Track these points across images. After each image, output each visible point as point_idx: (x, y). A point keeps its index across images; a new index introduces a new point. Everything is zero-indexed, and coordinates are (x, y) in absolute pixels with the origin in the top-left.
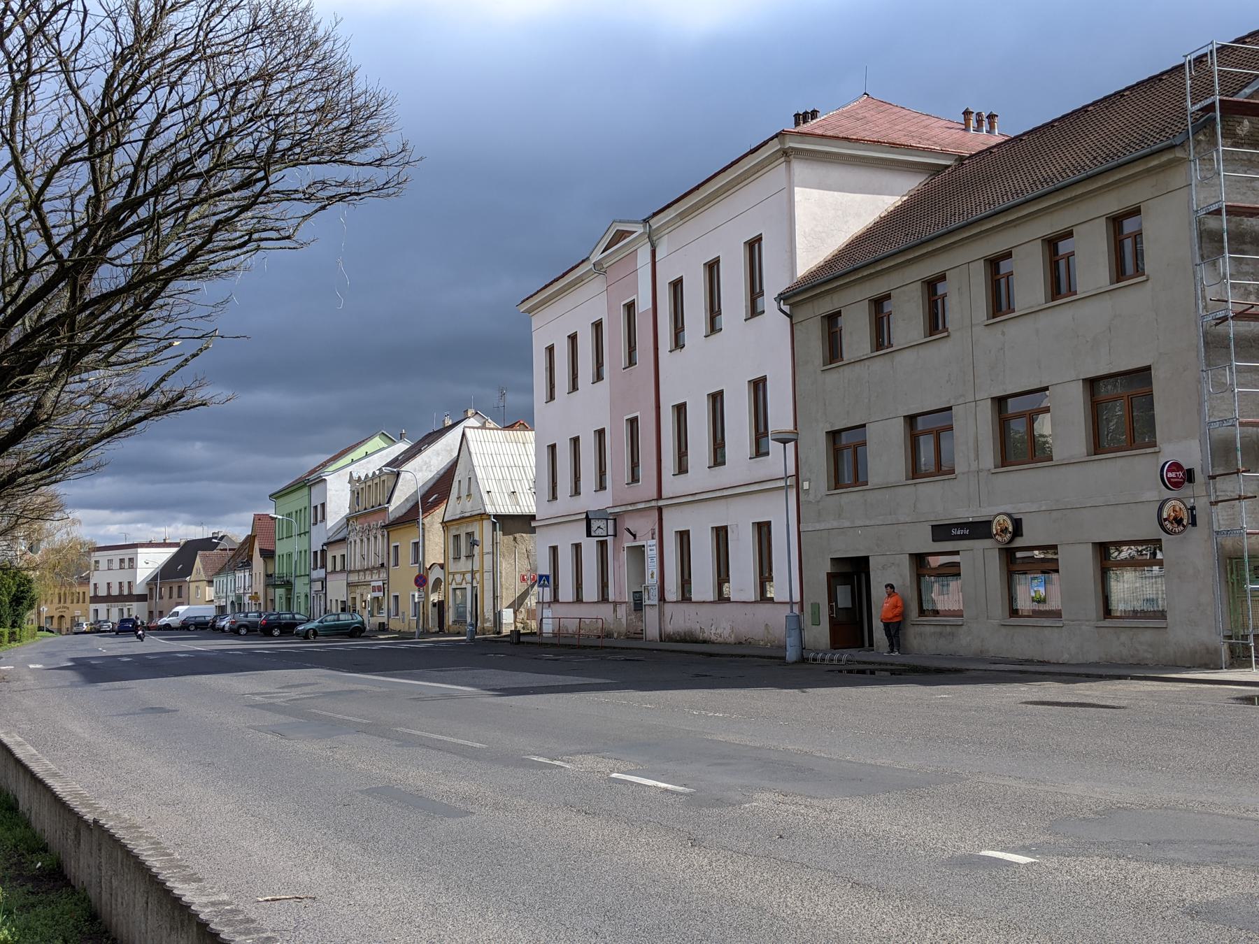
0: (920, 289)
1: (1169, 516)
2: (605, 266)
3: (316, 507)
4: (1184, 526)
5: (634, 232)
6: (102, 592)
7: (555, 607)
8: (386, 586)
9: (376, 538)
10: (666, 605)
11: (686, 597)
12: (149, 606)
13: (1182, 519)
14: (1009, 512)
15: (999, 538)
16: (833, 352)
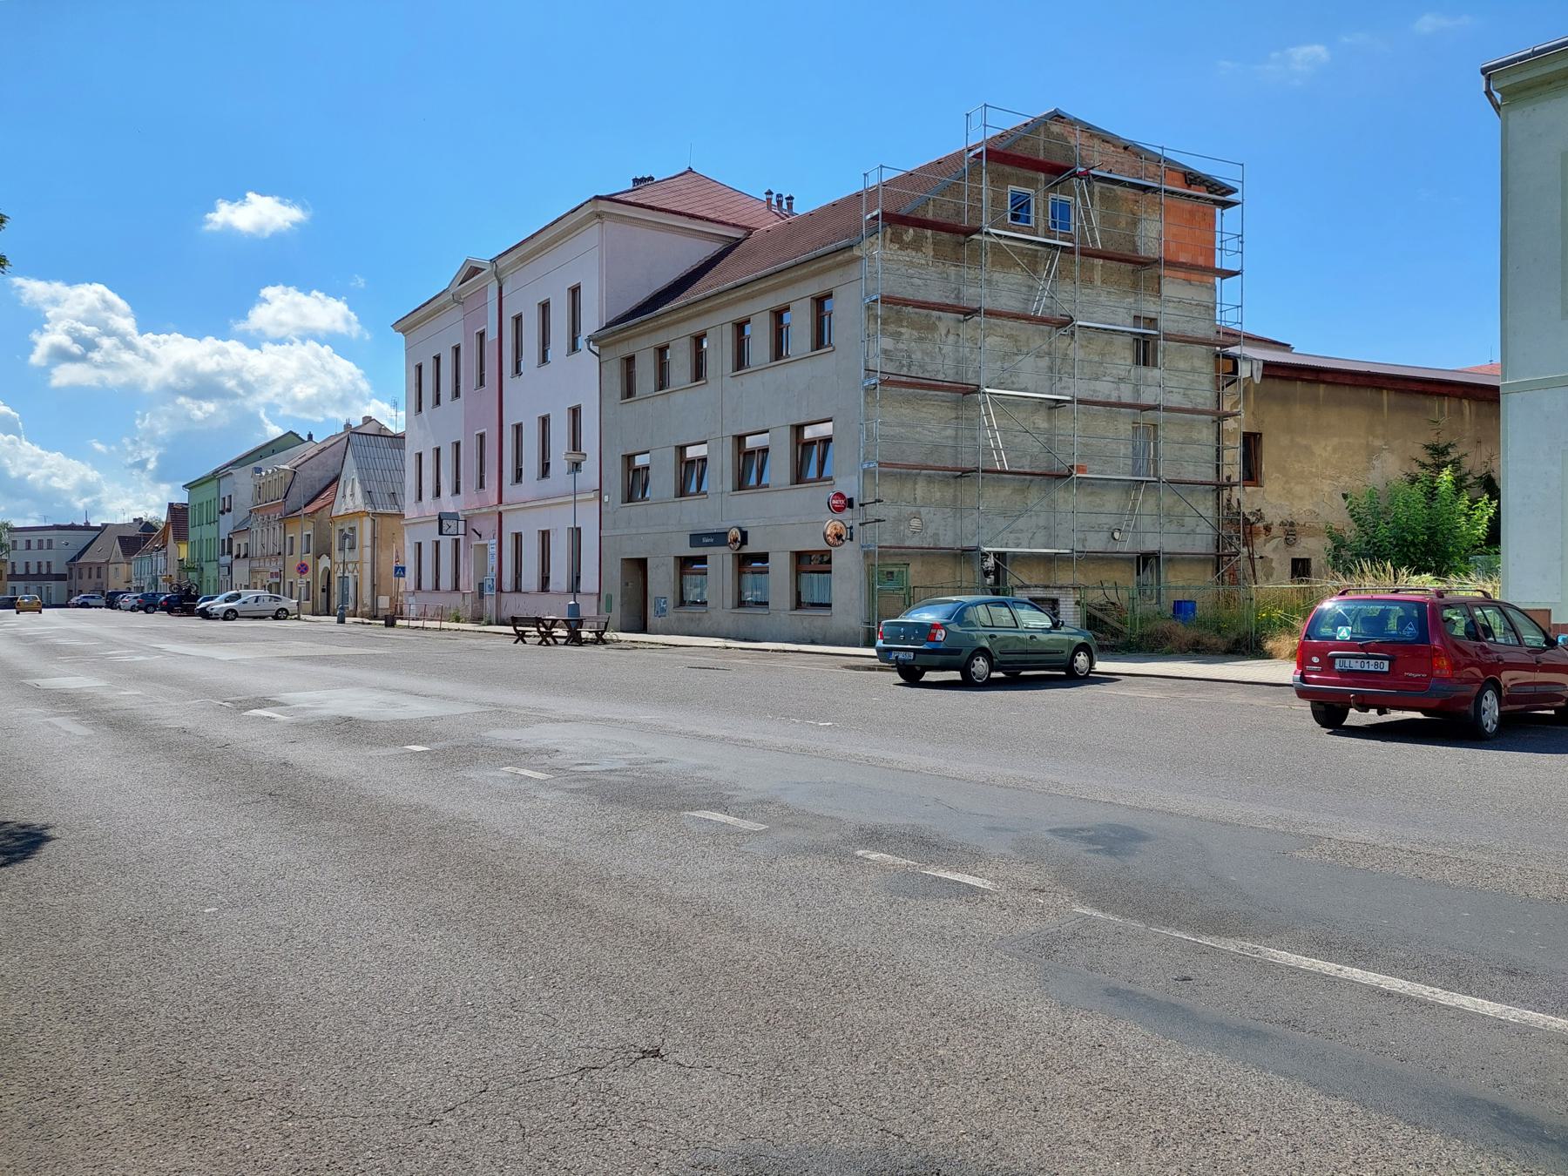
0: (689, 342)
1: (832, 532)
2: (463, 297)
3: (224, 499)
4: (843, 540)
5: (483, 270)
6: (20, 570)
7: (419, 595)
8: (282, 573)
9: (274, 529)
10: (503, 594)
11: (517, 589)
12: (69, 586)
13: (841, 536)
14: (741, 525)
15: (732, 545)
16: (629, 392)
